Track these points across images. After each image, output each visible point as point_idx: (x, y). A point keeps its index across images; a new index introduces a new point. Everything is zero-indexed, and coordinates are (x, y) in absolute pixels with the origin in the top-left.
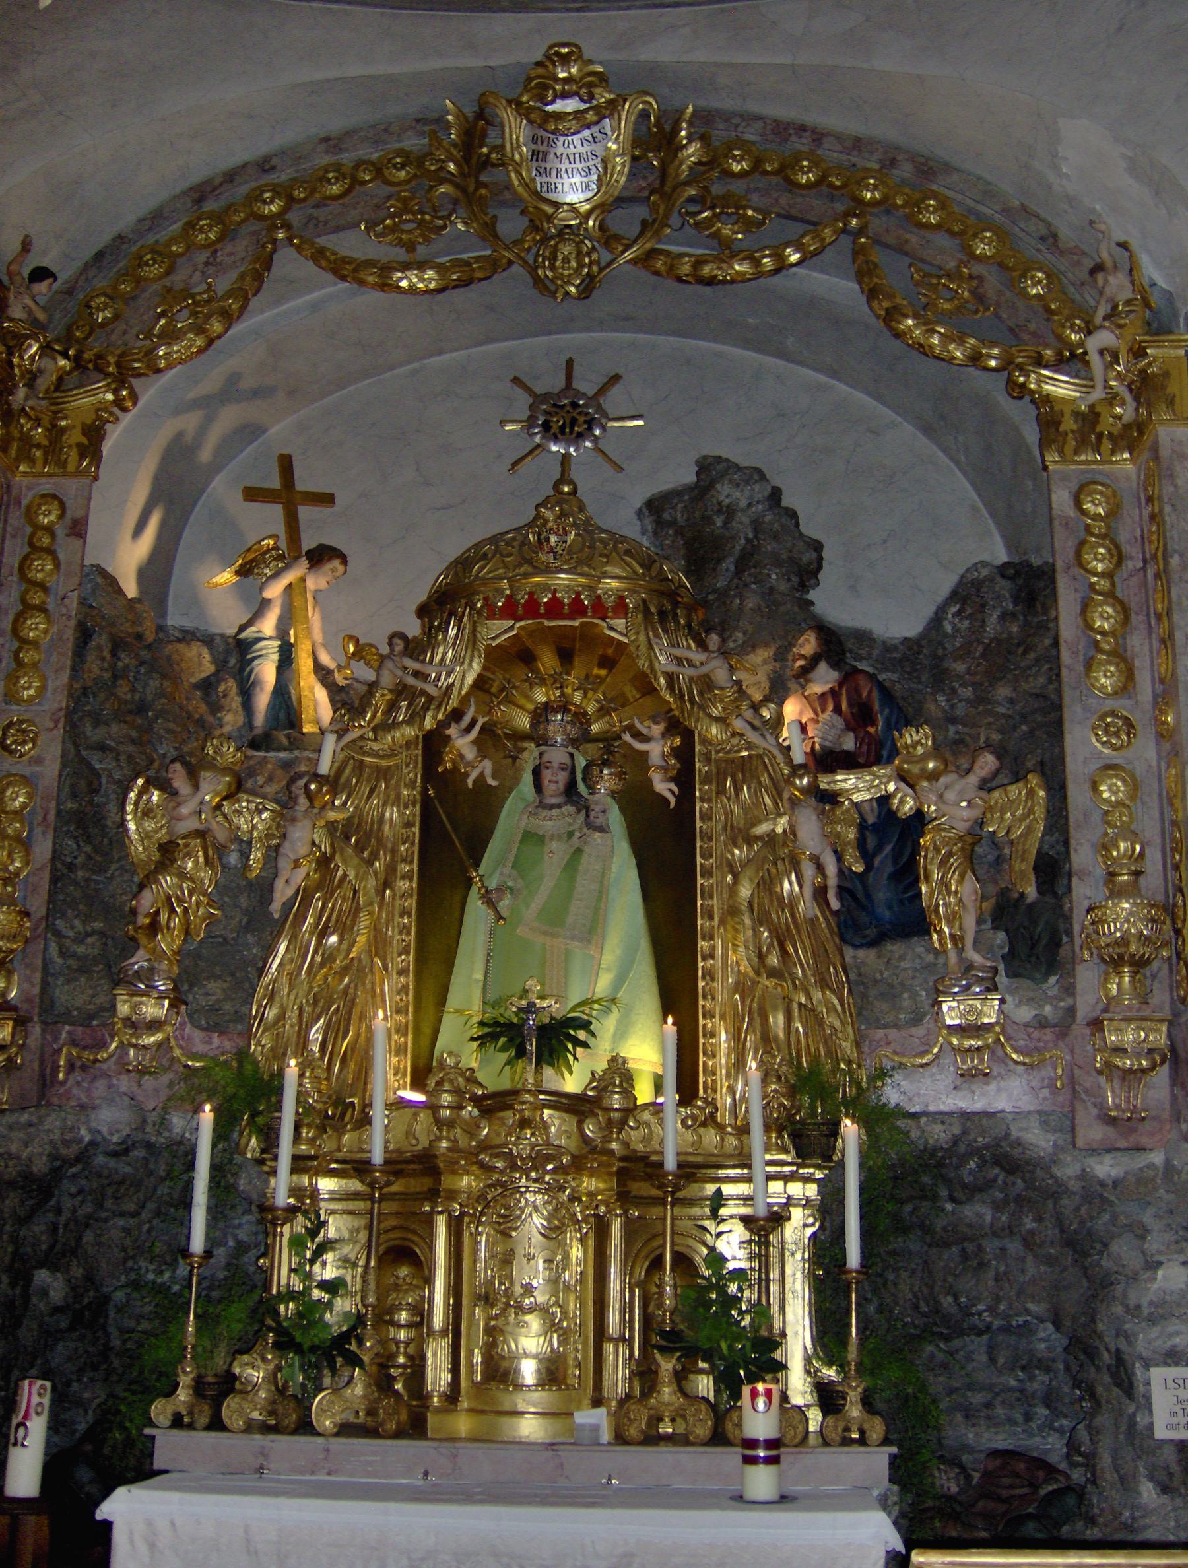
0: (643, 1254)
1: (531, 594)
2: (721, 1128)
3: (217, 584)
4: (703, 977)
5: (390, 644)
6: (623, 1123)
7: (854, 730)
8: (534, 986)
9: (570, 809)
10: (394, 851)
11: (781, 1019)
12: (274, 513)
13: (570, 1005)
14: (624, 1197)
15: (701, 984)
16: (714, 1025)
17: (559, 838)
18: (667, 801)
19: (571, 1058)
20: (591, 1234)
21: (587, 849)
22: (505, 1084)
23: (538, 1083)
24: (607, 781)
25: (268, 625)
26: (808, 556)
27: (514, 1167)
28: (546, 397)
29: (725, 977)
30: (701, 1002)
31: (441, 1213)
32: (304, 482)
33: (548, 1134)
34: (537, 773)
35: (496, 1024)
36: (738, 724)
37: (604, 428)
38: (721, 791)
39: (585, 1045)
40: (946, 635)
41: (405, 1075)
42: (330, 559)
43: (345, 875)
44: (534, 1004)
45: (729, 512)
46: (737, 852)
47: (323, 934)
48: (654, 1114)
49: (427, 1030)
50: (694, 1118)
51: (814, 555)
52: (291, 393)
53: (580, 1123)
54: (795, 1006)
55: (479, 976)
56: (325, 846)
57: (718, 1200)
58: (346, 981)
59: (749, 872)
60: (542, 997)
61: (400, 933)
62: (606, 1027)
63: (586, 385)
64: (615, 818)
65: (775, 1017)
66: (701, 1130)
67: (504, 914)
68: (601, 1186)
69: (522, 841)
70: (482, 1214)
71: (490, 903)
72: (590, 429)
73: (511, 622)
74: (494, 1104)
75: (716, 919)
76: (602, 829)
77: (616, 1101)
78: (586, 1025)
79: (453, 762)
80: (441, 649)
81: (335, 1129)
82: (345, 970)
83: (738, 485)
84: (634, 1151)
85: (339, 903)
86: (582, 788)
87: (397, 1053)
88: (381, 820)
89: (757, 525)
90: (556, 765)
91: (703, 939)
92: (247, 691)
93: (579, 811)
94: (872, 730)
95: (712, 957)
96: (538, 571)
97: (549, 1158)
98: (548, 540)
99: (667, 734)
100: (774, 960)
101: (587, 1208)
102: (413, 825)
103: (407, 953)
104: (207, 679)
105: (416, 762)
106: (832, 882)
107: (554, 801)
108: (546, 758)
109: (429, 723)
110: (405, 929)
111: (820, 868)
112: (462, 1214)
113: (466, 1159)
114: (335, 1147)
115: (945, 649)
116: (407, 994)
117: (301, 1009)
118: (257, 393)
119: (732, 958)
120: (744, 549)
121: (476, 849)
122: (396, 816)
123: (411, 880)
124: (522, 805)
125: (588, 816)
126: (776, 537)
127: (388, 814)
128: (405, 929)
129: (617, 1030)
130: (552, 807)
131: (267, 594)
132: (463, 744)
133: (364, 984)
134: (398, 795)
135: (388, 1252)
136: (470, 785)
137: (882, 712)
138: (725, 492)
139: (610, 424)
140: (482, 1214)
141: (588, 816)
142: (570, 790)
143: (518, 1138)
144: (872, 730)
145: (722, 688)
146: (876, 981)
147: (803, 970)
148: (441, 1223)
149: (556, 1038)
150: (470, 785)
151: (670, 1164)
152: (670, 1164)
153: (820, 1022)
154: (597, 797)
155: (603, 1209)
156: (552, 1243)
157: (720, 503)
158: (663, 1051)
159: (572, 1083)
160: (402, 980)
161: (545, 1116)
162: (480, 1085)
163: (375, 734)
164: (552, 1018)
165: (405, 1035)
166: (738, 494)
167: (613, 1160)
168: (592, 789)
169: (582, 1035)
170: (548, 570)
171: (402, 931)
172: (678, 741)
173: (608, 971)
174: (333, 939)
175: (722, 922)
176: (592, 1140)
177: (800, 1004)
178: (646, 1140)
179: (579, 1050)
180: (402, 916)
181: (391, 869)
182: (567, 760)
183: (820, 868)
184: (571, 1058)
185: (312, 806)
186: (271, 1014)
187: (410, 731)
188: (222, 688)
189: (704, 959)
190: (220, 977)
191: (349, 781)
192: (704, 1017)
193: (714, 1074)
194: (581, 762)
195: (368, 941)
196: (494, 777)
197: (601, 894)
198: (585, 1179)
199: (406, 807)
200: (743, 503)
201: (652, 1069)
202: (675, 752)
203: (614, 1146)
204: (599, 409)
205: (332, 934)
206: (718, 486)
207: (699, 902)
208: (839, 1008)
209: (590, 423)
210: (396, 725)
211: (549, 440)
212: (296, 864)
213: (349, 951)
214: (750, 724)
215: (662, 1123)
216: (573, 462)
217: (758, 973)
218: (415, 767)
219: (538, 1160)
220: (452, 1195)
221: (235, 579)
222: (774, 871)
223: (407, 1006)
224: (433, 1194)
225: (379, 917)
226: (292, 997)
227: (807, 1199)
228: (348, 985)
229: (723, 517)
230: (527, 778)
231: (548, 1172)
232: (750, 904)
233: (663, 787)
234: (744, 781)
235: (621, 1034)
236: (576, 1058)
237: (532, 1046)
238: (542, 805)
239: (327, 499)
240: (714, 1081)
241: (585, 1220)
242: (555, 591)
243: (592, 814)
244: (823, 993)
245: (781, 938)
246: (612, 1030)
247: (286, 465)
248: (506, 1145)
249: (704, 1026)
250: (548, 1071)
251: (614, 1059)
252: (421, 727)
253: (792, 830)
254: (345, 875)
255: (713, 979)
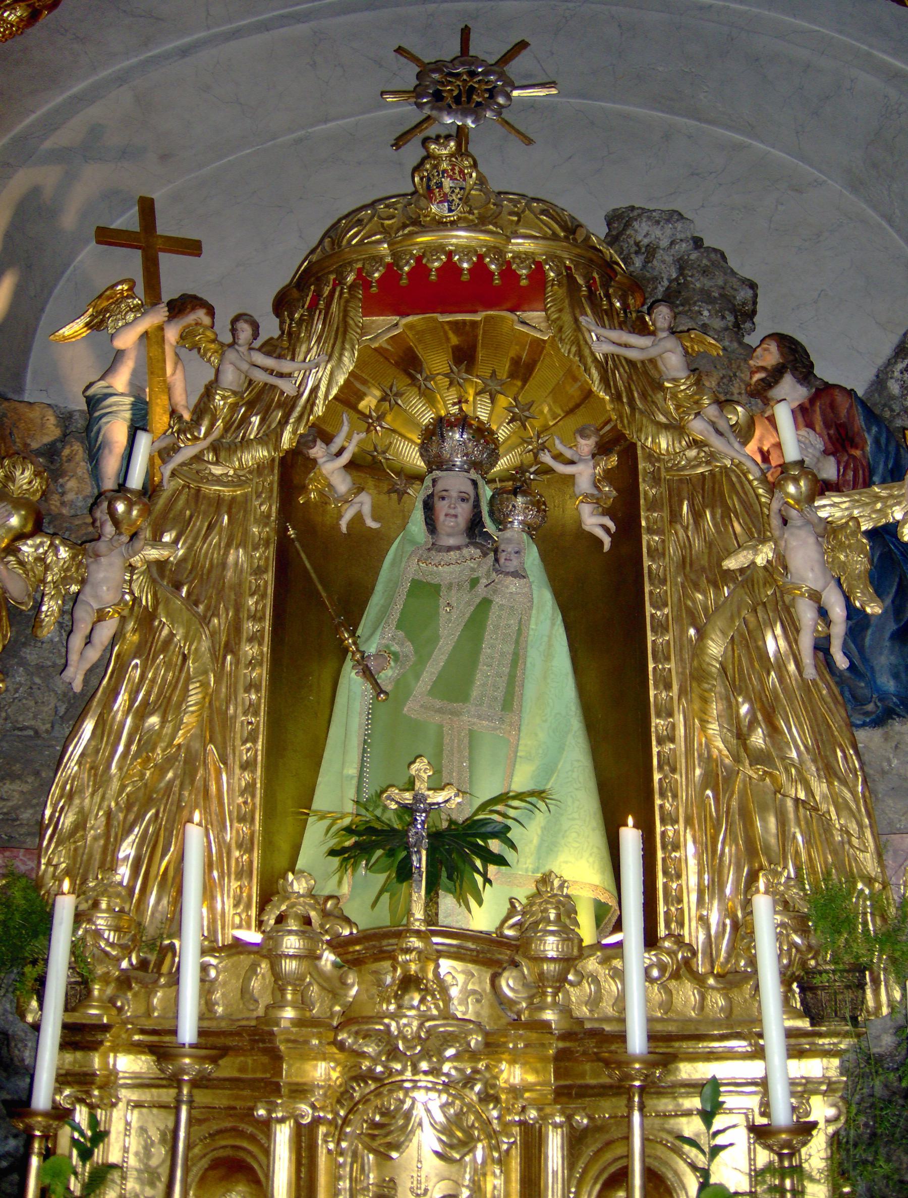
0: (593, 1172)
1: (419, 259)
2: (699, 980)
3: (65, 338)
4: (660, 768)
5: (234, 331)
6: (561, 980)
7: (833, 454)
8: (421, 769)
9: (475, 552)
10: (238, 607)
11: (772, 821)
12: (132, 263)
13: (477, 803)
14: (567, 1094)
15: (657, 776)
16: (677, 832)
17: (460, 586)
18: (601, 543)
19: (479, 879)
20: (515, 1153)
21: (497, 600)
22: (382, 917)
23: (431, 918)
24: (520, 512)
25: (121, 381)
26: (744, 294)
27: (393, 1053)
28: (437, 66)
29: (690, 769)
30: (658, 802)
31: (282, 1120)
32: (165, 227)
33: (447, 999)
34: (429, 507)
35: (370, 830)
36: (698, 427)
37: (508, 97)
38: (675, 516)
39: (501, 861)
40: (892, 398)
41: (248, 906)
42: (193, 309)
43: (172, 635)
44: (425, 798)
45: (651, 251)
46: (700, 596)
47: (142, 715)
48: (605, 961)
49: (284, 845)
50: (662, 967)
51: (750, 293)
52: (164, 158)
53: (495, 978)
54: (790, 803)
55: (352, 770)
56: (147, 599)
57: (712, 1097)
58: (170, 775)
59: (720, 623)
60: (438, 788)
61: (245, 713)
62: (528, 835)
63: (487, 48)
64: (532, 558)
65: (764, 820)
66: (673, 984)
67: (388, 688)
68: (531, 1078)
69: (410, 593)
70: (346, 1121)
71: (368, 674)
72: (492, 97)
73: (395, 319)
74: (367, 950)
75: (675, 687)
76: (518, 574)
77: (551, 946)
78: (502, 833)
79: (321, 493)
80: (304, 348)
81: (144, 984)
82: (169, 761)
83: (658, 222)
84: (580, 1021)
85: (160, 672)
86: (490, 527)
87: (239, 876)
88: (224, 565)
89: (682, 265)
90: (454, 494)
91: (658, 716)
92: (94, 455)
93: (485, 555)
94: (857, 453)
95: (672, 740)
96: (424, 229)
97: (448, 1039)
98: (440, 186)
99: (602, 449)
100: (758, 739)
101: (509, 1111)
102: (266, 571)
103: (255, 741)
104: (53, 444)
105: (271, 490)
106: (839, 630)
107: (451, 542)
108: (440, 486)
109: (287, 439)
110: (253, 709)
111: (823, 613)
112: (316, 1121)
113: (319, 1036)
114: (142, 1010)
115: (892, 410)
116: (253, 796)
117: (109, 815)
118: (125, 153)
119: (699, 740)
120: (668, 288)
121: (352, 607)
122: (246, 562)
123: (260, 644)
124: (409, 549)
125: (497, 560)
126: (705, 272)
127: (231, 559)
128: (253, 709)
129: (542, 840)
130: (449, 549)
131: (120, 343)
132: (331, 469)
133: (192, 782)
134: (246, 532)
135: (215, 1165)
136: (344, 529)
137: (869, 431)
138: (642, 231)
139: (515, 93)
140: (346, 1121)
141: (497, 560)
142: (474, 527)
143: (400, 1007)
144: (857, 453)
145: (674, 380)
146: (883, 773)
147: (799, 753)
148: (283, 1135)
149: (462, 850)
150: (344, 529)
151: (637, 1041)
152: (637, 1041)
153: (827, 827)
154: (508, 534)
155: (533, 1113)
156: (454, 1168)
157: (637, 244)
158: (603, 873)
159: (483, 917)
160: (247, 776)
161: (442, 971)
162: (348, 921)
163: (216, 454)
164: (451, 822)
165: (250, 851)
166: (658, 233)
167: (547, 1039)
168: (501, 522)
169: (495, 845)
170: (440, 224)
171: (249, 712)
172: (614, 460)
173: (536, 738)
174: (154, 720)
175: (682, 692)
176: (513, 1002)
177: (797, 800)
178: (594, 1001)
179: (492, 869)
180: (247, 690)
181: (236, 628)
182: (469, 489)
183: (823, 613)
184: (479, 879)
185: (119, 533)
186: (68, 821)
187: (262, 453)
188: (66, 452)
189: (659, 743)
190: (19, 777)
191: (182, 512)
192: (663, 822)
193: (680, 901)
194: (487, 492)
195: (200, 722)
196: (375, 519)
197: (520, 637)
198: (504, 1066)
199: (256, 548)
200: (664, 243)
201: (592, 895)
202: (609, 476)
203: (549, 1015)
204: (502, 76)
205: (151, 714)
206: (636, 224)
207: (651, 666)
208: (854, 807)
209: (492, 93)
210: (246, 444)
211: (440, 109)
212: (101, 616)
213: (173, 736)
214: (713, 424)
215: (619, 975)
216: (471, 136)
217: (737, 760)
218: (270, 497)
219: (431, 1045)
220: (300, 1091)
221: (85, 332)
222: (751, 619)
223: (253, 812)
224: (270, 1088)
225: (217, 691)
226: (97, 799)
227: (830, 1084)
228: (171, 782)
229: (642, 257)
230: (418, 515)
231: (448, 1059)
232: (724, 668)
233: (595, 522)
234: (704, 507)
235: (550, 844)
236: (487, 881)
237: (420, 861)
238: (435, 547)
239: (193, 248)
240: (681, 910)
241: (506, 1126)
242: (450, 255)
243: (502, 557)
244: (830, 784)
245: (768, 712)
246: (536, 841)
247: (147, 208)
248: (379, 1018)
249: (663, 834)
250: (447, 902)
251: (545, 880)
252: (277, 447)
253: (781, 561)
254: (172, 635)
255: (674, 770)
